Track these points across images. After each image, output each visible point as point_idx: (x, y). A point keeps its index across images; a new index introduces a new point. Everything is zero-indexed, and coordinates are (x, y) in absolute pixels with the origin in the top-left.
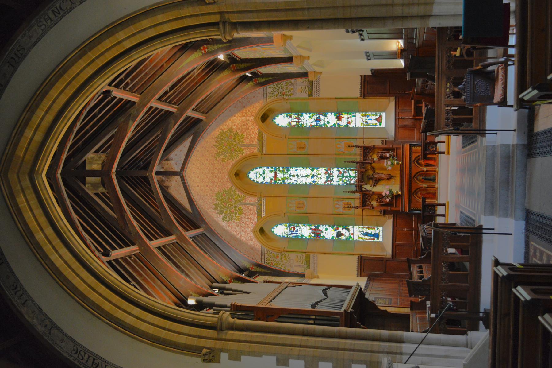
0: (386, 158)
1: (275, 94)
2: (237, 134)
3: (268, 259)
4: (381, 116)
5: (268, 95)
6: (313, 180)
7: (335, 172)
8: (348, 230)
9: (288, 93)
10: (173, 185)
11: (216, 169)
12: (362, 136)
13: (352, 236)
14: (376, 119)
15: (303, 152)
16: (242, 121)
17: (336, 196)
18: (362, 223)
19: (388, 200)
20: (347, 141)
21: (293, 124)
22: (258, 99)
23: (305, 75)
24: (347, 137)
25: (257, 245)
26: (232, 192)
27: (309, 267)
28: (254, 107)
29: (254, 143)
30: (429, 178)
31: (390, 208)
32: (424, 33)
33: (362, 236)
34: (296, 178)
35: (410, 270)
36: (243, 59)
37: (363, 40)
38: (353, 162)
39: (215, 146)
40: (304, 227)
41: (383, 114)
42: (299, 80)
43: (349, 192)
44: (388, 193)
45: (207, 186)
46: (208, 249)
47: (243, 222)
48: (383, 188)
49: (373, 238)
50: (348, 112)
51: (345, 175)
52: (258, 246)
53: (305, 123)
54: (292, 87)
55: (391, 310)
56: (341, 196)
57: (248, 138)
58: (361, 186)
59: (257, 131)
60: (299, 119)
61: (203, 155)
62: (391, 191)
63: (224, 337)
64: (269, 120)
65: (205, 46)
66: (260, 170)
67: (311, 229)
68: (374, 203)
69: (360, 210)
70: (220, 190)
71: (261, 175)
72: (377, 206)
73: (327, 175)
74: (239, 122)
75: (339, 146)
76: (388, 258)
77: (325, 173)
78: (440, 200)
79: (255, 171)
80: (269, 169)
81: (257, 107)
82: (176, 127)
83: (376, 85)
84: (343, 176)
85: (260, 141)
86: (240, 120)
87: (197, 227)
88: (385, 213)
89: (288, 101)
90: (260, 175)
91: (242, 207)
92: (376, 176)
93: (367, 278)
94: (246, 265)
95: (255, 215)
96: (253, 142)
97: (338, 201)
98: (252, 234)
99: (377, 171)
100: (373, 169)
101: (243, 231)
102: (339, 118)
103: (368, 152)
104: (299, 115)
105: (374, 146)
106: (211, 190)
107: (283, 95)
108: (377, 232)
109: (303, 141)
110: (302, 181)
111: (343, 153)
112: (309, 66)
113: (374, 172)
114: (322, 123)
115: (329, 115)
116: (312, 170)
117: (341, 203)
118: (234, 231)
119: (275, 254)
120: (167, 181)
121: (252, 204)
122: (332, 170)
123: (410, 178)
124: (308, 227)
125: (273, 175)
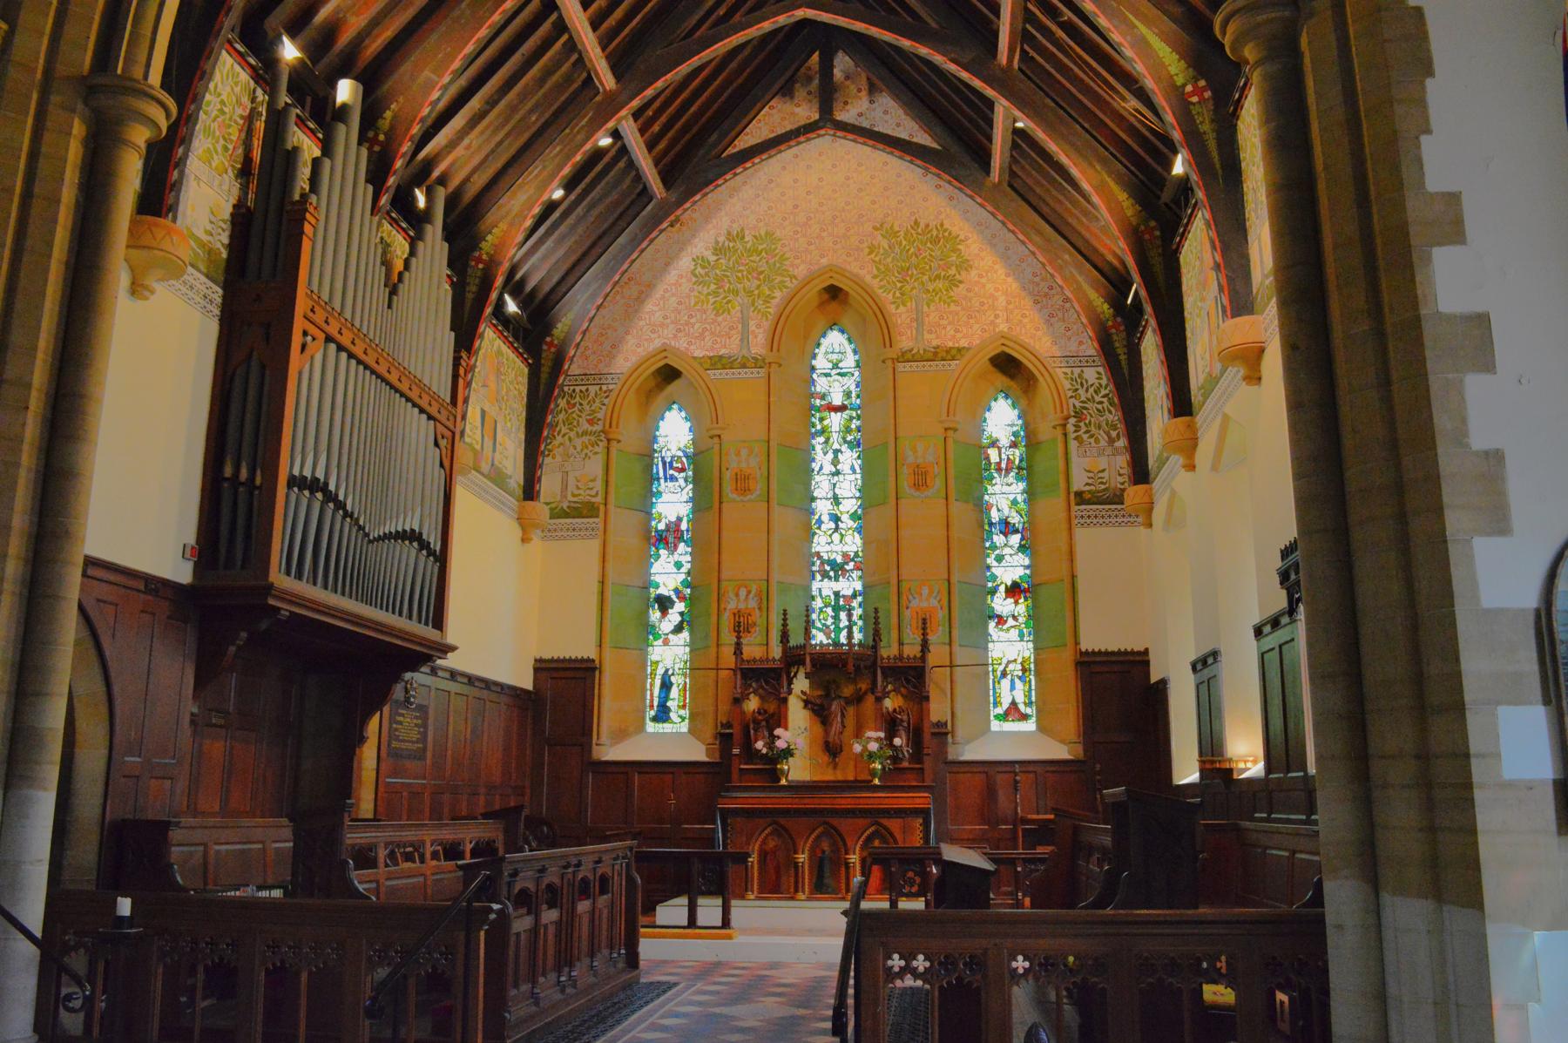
0: (891, 735)
1: (1081, 392)
2: (954, 283)
3: (584, 394)
4: (1024, 717)
6: (825, 518)
7: (850, 585)
8: (678, 629)
9: (1084, 429)
10: (797, 110)
11: (848, 229)
12: (958, 660)
13: (660, 642)
14: (1014, 704)
15: (905, 483)
17: (774, 588)
19: (759, 745)
20: (942, 615)
21: (993, 454)
22: (1058, 341)
23: (1141, 473)
24: (956, 613)
25: (626, 360)
26: (779, 279)
27: (558, 514)
28: (1037, 329)
29: (927, 336)
30: (827, 874)
31: (740, 746)
32: (1294, 852)
33: (660, 671)
34: (828, 468)
35: (485, 816)
36: (1177, 260)
37: (1258, 632)
38: (877, 635)
39: (916, 222)
40: (685, 498)
41: (1030, 726)
42: (1122, 461)
43: (785, 625)
44: (781, 744)
45: (796, 206)
46: (601, 208)
47: (691, 316)
48: (797, 728)
50: (1034, 616)
53: (997, 489)
54: (1103, 443)
55: (368, 756)
57: (942, 318)
58: (804, 664)
59: (964, 343)
60: (1008, 471)
61: (886, 189)
62: (788, 753)
63: (55, 99)
64: (1001, 380)
65: (1208, 94)
66: (849, 362)
67: (679, 519)
68: (752, 704)
69: (729, 659)
70: (783, 245)
71: (835, 366)
72: (743, 713)
73: (839, 559)
75: (925, 591)
76: (590, 751)
77: (845, 555)
78: (739, 910)
79: (848, 348)
80: (853, 387)
82: (952, 67)
83: (1118, 697)
84: (837, 609)
85: (935, 354)
86: (997, 290)
87: (667, 179)
88: (724, 739)
89: (1059, 431)
90: (836, 361)
91: (736, 310)
92: (835, 706)
93: (530, 687)
94: (559, 325)
95: (712, 349)
96: (930, 332)
97: (759, 594)
99: (851, 710)
100: (858, 699)
101: (666, 317)
102: (1014, 590)
103: (908, 681)
104: (1020, 468)
105: (927, 698)
106: (784, 219)
107: (1079, 415)
109: (939, 483)
110: (821, 486)
111: (904, 602)
112: (1171, 479)
113: (848, 701)
114: (999, 539)
116: (854, 516)
117: (752, 604)
118: (666, 291)
119: (600, 415)
120: (809, 93)
121: (744, 339)
122: (856, 574)
123: (821, 812)
124: (684, 510)
125: (837, 400)
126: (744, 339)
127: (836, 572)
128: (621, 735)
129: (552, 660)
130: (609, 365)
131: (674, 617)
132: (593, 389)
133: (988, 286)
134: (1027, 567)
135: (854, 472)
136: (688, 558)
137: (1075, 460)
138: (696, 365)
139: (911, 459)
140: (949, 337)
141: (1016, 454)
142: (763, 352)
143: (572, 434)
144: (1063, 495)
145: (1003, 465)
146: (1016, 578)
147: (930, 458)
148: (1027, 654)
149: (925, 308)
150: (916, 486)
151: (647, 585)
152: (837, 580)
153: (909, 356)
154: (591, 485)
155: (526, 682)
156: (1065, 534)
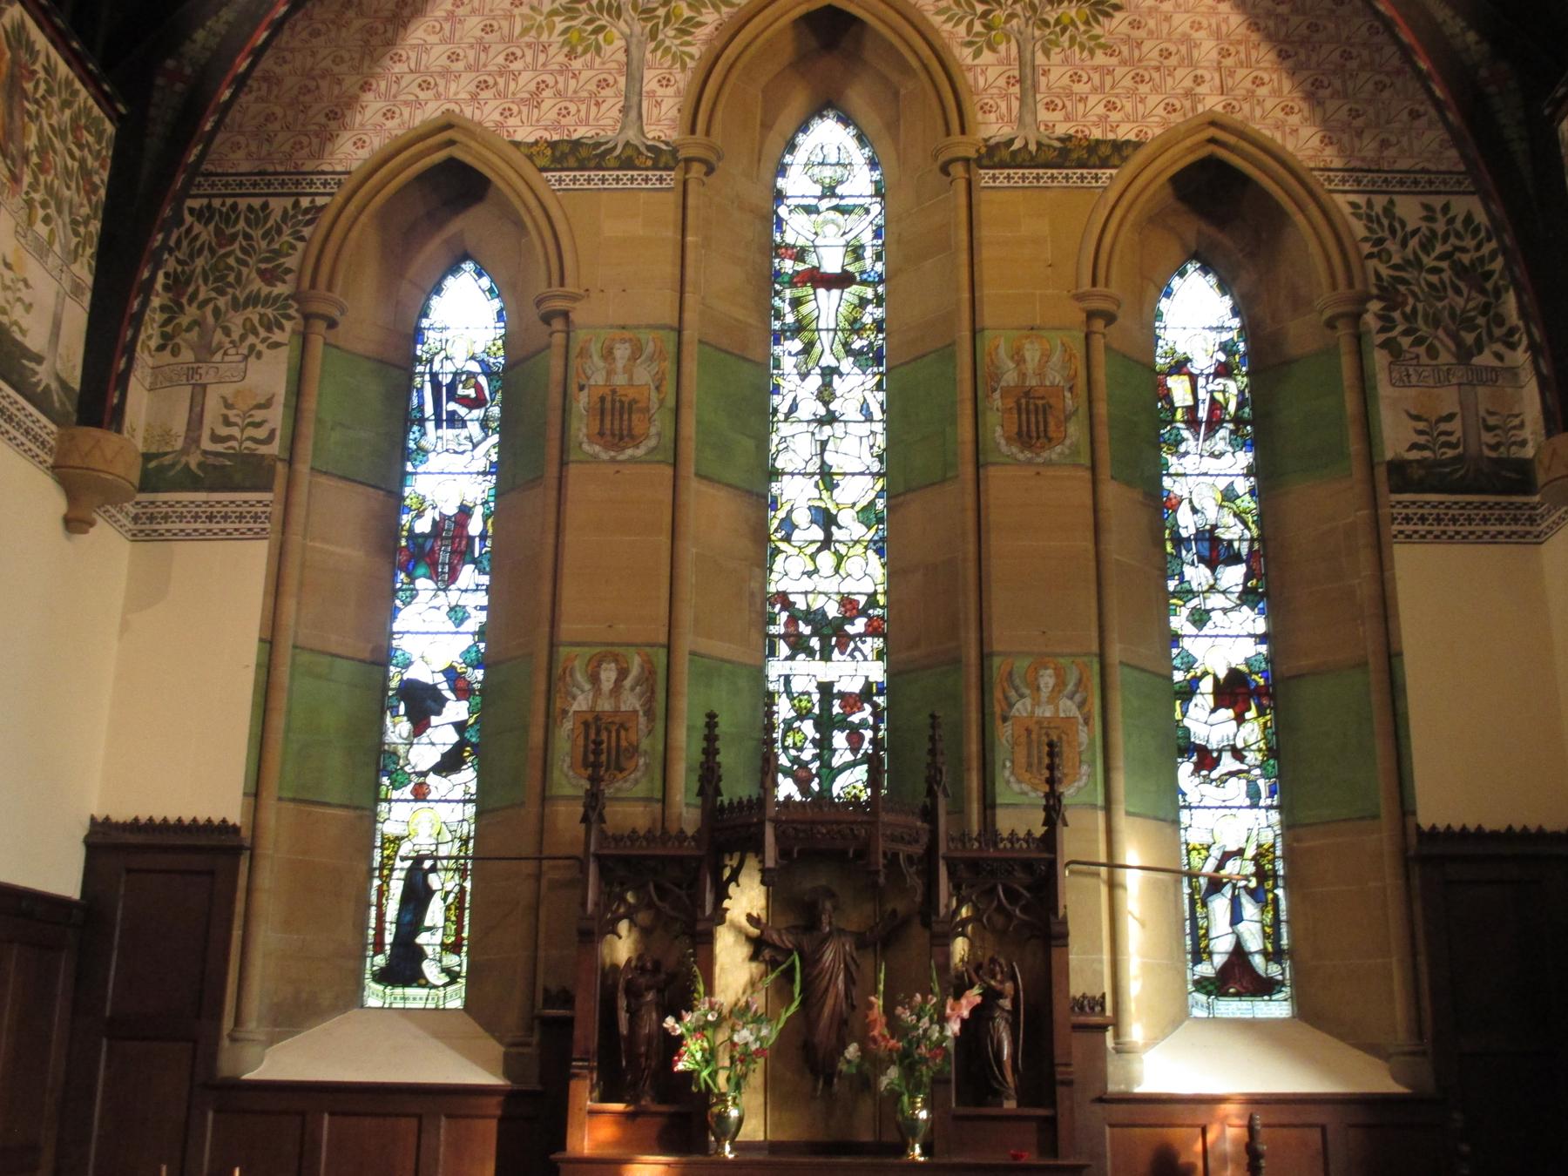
3: (258, 217)
4: (1264, 988)
5: (1380, 201)
6: (802, 517)
7: (859, 669)
8: (449, 764)
13: (406, 792)
14: (1239, 952)
15: (997, 432)
16: (1186, 38)
17: (683, 665)
18: (486, 854)
21: (1179, 389)
25: (360, 143)
28: (1288, 111)
29: (1043, 115)
34: (810, 407)
40: (481, 464)
43: (710, 751)
49: (389, 938)
51: (839, 739)
52: (350, 152)
53: (1189, 464)
54: (1445, 358)
56: (683, 704)
59: (1126, 132)
60: (1213, 425)
66: (860, 183)
67: (465, 511)
69: (567, 816)
71: (829, 191)
74: (1181, 22)
75: (1047, 680)
76: (213, 1056)
77: (846, 601)
79: (859, 156)
80: (867, 238)
81: (1283, 122)
84: (826, 724)
86: (1196, 26)
89: (1343, 333)
91: (614, 50)
94: (200, 35)
95: (556, 126)
97: (648, 676)
98: (432, 111)
101: (454, 57)
102: (1233, 691)
104: (1238, 420)
107: (1389, 294)
108: (430, 970)
109: (1075, 431)
110: (793, 446)
114: (1197, 575)
115: (1253, 621)
116: (867, 514)
117: (631, 701)
119: (291, 262)
121: (631, 108)
122: (872, 645)
125: (832, 262)
126: (631, 108)
127: (824, 640)
128: (294, 1016)
129: (135, 826)
130: (318, 155)
131: (441, 734)
132: (277, 205)
133: (1178, 19)
134: (1262, 639)
135: (869, 418)
136: (482, 598)
137: (1385, 390)
138: (517, 157)
139: (1010, 378)
140: (1091, 119)
141: (1231, 390)
142: (674, 136)
143: (222, 302)
144: (1358, 470)
145: (1203, 413)
146: (1238, 662)
147: (1055, 377)
148: (1267, 837)
149: (1040, 58)
150: (1025, 438)
151: (382, 656)
152: (826, 656)
153: (1005, 154)
154: (259, 415)
155: (62, 876)
156: (1365, 558)
